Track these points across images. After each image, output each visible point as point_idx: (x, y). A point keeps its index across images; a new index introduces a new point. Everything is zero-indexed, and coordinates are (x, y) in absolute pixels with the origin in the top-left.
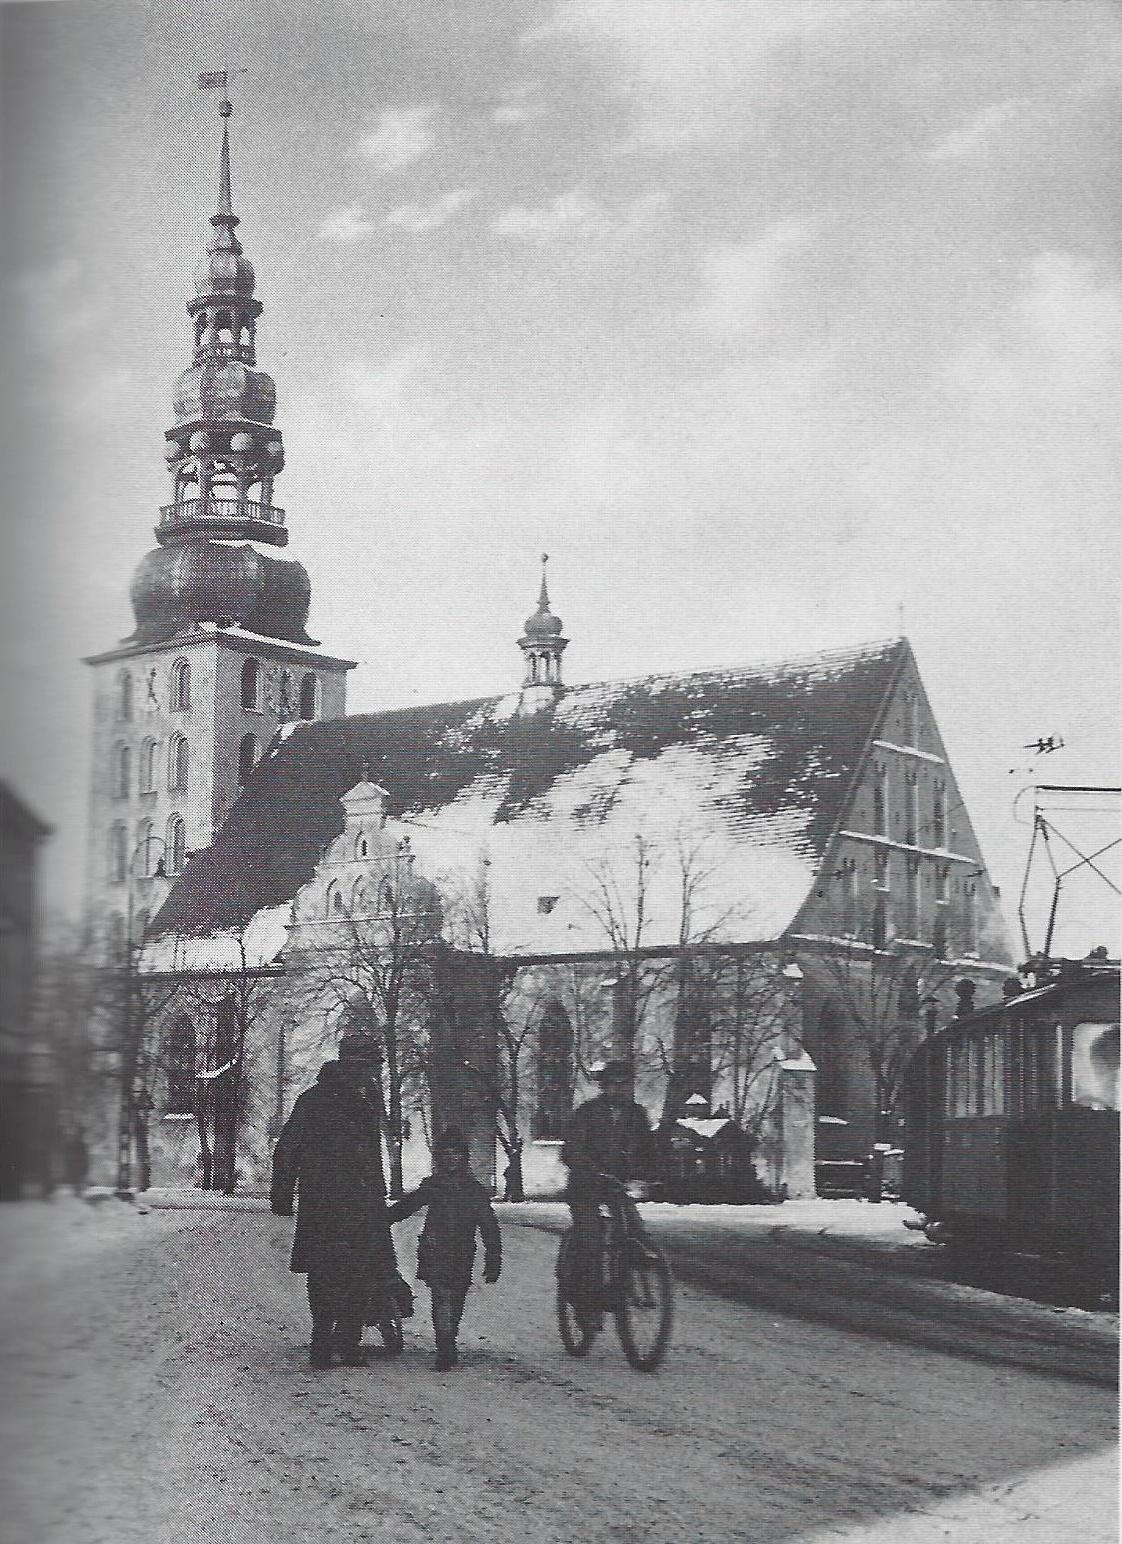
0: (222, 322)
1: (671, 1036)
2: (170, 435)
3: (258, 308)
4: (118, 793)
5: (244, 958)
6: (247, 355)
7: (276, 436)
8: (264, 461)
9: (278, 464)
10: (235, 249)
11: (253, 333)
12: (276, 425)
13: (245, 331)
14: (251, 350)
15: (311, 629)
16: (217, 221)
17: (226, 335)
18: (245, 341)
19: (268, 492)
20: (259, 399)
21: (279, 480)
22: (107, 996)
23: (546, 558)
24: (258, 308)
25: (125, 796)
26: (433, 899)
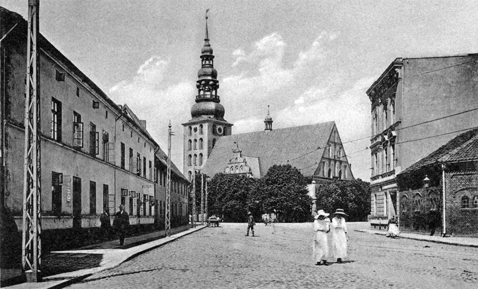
0: (207, 59)
1: (157, 233)
2: (198, 82)
3: (213, 57)
4: (246, 234)
5: (421, 240)
6: (212, 66)
7: (218, 82)
8: (215, 86)
9: (218, 87)
10: (209, 46)
11: (213, 62)
12: (217, 79)
13: (211, 61)
14: (212, 65)
15: (225, 118)
16: (205, 40)
17: (207, 62)
18: (211, 63)
19: (216, 93)
20: (214, 74)
21: (218, 90)
22: (444, 157)
23: (269, 106)
24: (213, 57)
25: (248, 235)
26: (308, 64)
